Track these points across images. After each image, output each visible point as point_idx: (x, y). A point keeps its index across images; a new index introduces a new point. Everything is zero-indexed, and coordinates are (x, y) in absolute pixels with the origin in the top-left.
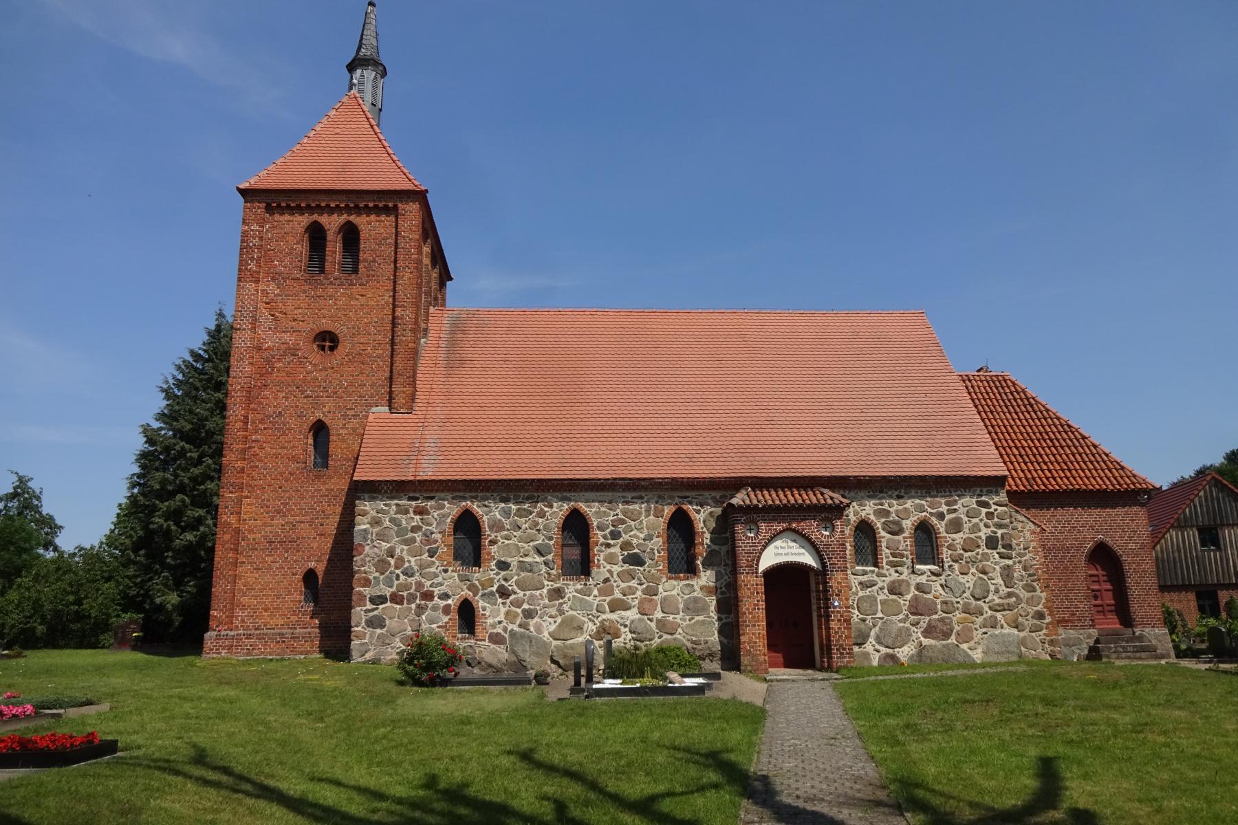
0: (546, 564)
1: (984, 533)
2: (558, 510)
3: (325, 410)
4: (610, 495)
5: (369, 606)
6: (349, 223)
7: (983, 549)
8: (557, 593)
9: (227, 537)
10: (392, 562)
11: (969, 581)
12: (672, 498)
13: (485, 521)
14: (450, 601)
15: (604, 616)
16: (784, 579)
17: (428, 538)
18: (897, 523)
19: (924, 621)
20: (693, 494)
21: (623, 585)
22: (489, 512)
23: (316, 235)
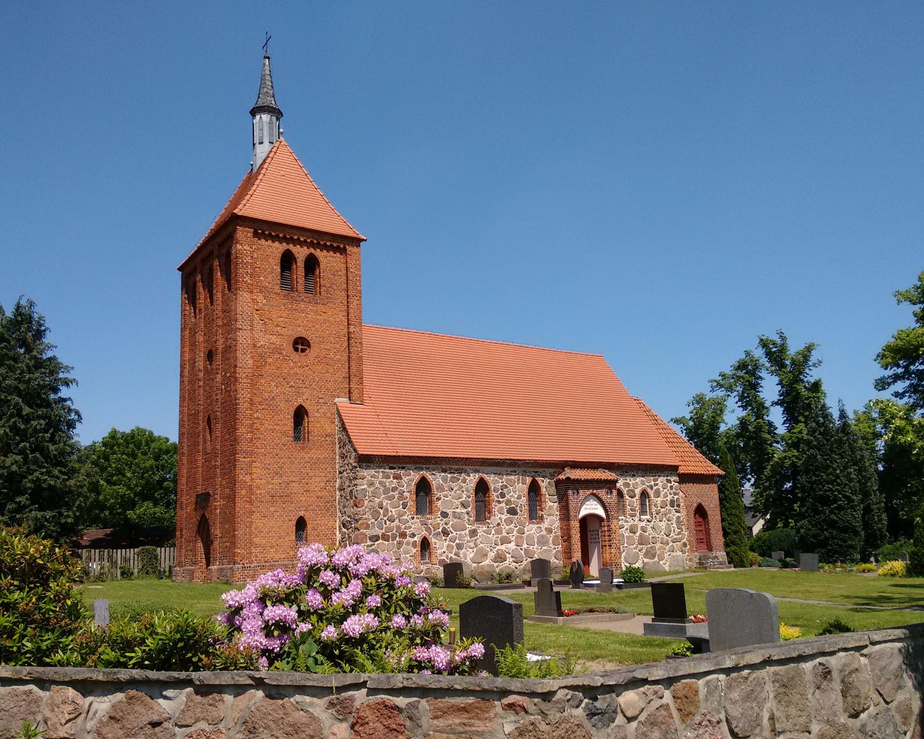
0: (468, 513)
1: (669, 498)
2: (412, 477)
3: (305, 397)
4: (499, 469)
5: (369, 543)
6: (311, 255)
7: (669, 507)
8: (473, 533)
9: (243, 492)
10: (382, 511)
11: (663, 525)
12: (530, 472)
13: (434, 484)
14: (416, 539)
15: (498, 547)
16: (585, 522)
17: (401, 496)
18: (633, 491)
19: (645, 547)
20: (540, 470)
21: (507, 527)
22: (436, 479)
23: (287, 260)
